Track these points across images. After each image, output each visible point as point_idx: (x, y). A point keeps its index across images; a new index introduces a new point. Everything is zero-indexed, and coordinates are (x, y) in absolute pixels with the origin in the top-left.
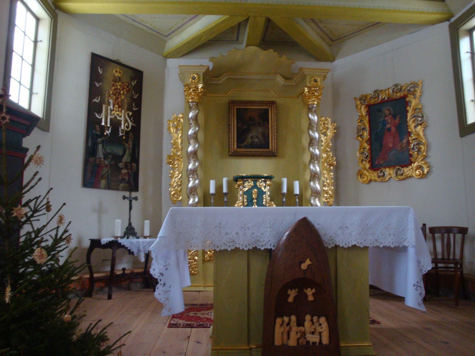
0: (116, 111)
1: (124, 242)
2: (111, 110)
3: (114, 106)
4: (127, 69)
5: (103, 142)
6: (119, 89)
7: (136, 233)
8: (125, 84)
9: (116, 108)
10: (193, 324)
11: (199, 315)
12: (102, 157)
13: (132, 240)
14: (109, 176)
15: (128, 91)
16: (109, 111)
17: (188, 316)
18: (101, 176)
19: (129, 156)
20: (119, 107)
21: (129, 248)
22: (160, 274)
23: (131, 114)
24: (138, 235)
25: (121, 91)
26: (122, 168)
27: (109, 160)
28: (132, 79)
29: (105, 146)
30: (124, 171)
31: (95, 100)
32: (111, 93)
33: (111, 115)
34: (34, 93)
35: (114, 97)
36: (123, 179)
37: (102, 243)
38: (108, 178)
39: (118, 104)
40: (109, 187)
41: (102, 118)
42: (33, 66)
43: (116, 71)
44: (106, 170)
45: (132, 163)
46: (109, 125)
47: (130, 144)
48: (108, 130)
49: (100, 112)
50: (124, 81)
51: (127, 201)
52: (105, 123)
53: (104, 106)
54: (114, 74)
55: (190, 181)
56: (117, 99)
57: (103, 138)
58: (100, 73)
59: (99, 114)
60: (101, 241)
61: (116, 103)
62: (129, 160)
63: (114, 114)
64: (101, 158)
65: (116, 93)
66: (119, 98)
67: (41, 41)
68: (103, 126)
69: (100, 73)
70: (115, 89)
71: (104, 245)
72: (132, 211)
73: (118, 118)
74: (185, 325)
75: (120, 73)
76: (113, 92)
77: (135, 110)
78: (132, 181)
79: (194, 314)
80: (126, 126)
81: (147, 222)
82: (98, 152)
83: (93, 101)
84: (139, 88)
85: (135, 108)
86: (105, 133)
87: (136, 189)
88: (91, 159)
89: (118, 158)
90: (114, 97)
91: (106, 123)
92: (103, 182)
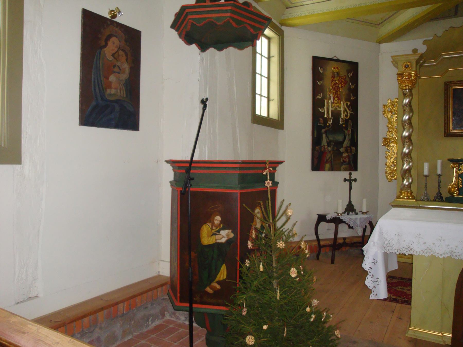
0: (336, 104)
1: (345, 218)
2: (332, 103)
3: (334, 99)
4: (344, 64)
5: (326, 132)
6: (338, 83)
7: (355, 210)
8: (342, 78)
9: (336, 101)
10: (399, 300)
11: (405, 291)
12: (326, 144)
13: (352, 216)
14: (332, 160)
15: (345, 84)
16: (330, 104)
17: (395, 290)
18: (325, 161)
19: (349, 141)
20: (339, 99)
21: (348, 224)
22: (370, 268)
23: (349, 103)
24: (357, 211)
25: (339, 85)
26: (343, 152)
27: (332, 146)
28: (348, 72)
29: (328, 135)
30: (345, 155)
31: (318, 97)
32: (331, 88)
33: (332, 107)
34: (271, 100)
35: (334, 92)
36: (344, 162)
37: (327, 219)
38: (331, 163)
39: (337, 97)
40: (332, 169)
41: (325, 111)
42: (269, 78)
43: (334, 68)
44: (330, 155)
45: (352, 147)
46: (330, 116)
47: (349, 132)
48: (330, 121)
49: (323, 106)
50: (341, 76)
51: (347, 183)
52: (327, 115)
53: (326, 101)
54: (333, 71)
55: (404, 163)
56: (337, 92)
57: (326, 129)
58: (321, 73)
59: (322, 108)
60: (327, 217)
61: (336, 96)
62: (348, 145)
63: (334, 106)
64: (325, 146)
65: (335, 88)
66: (338, 91)
67: (273, 56)
68: (326, 118)
69: (321, 73)
70: (335, 84)
71: (329, 220)
72: (351, 191)
73: (338, 109)
74: (392, 299)
75: (338, 68)
76: (332, 87)
77: (353, 100)
78: (352, 163)
79: (402, 289)
80: (346, 115)
81: (365, 201)
82: (323, 139)
83: (317, 98)
84: (355, 79)
85: (352, 98)
86: (328, 124)
87: (356, 169)
88: (317, 147)
89: (339, 144)
90: (334, 92)
91: (328, 115)
92: (327, 166)
